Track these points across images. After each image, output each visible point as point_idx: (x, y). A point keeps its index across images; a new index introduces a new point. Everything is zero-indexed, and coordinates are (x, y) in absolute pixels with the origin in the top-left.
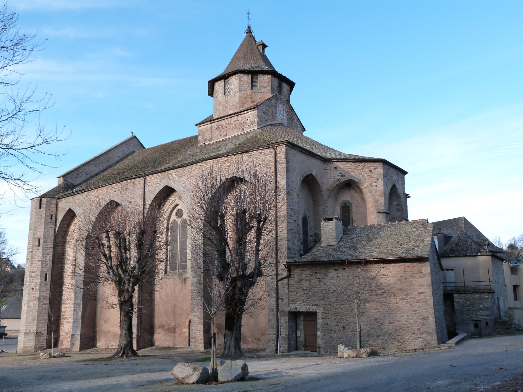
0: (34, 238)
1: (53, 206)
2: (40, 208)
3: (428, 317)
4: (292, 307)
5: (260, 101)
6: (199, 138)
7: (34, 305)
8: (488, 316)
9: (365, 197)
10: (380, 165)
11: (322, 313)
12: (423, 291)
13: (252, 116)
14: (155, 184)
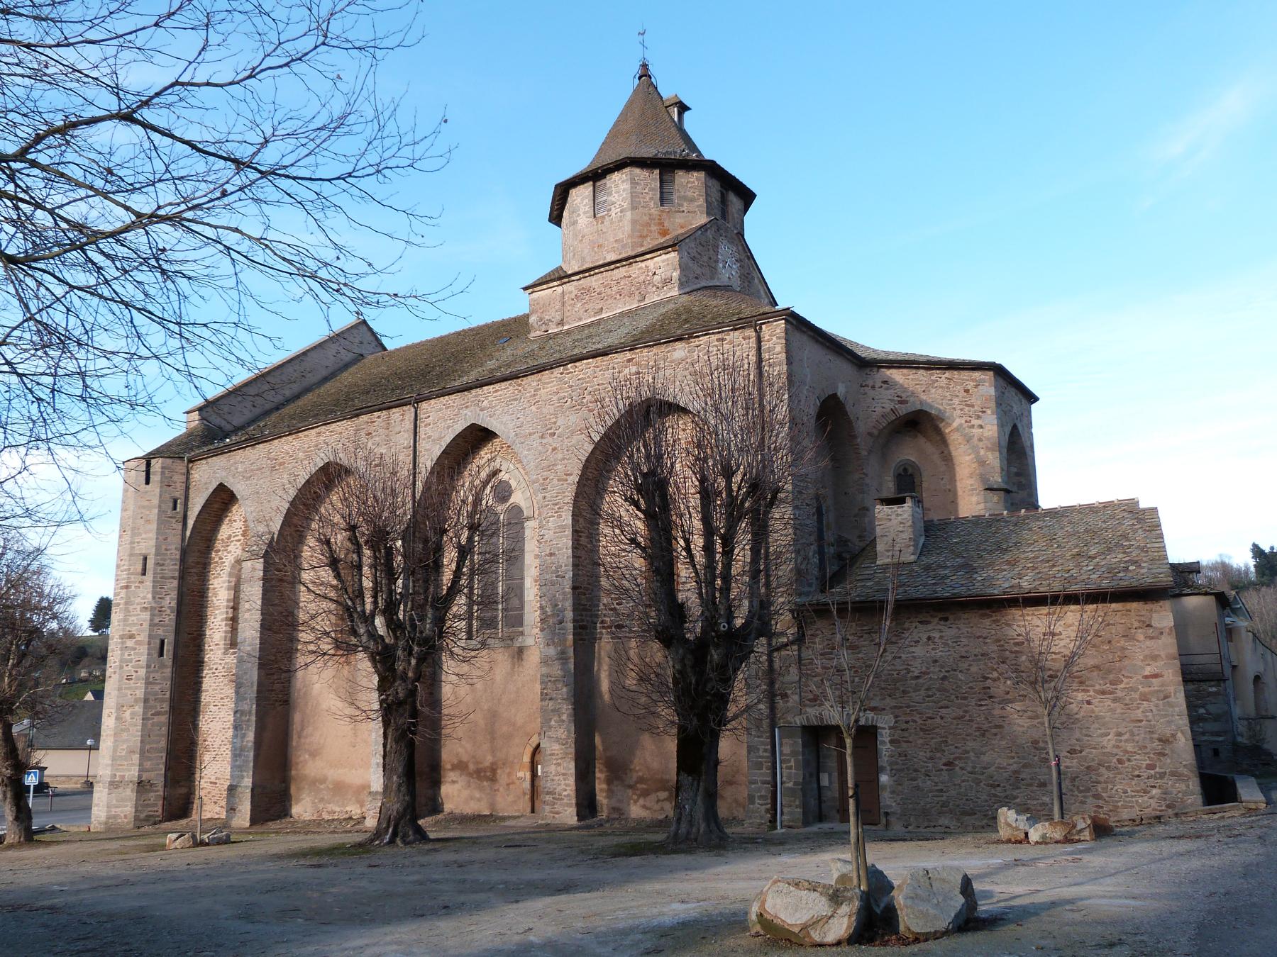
0: (131, 555)
1: (179, 479)
2: (147, 482)
3: (1173, 736)
4: (812, 714)
5: (682, 231)
6: (533, 319)
7: (133, 715)
8: (1218, 734)
9: (954, 453)
10: (988, 376)
11: (890, 728)
12: (1157, 671)
13: (666, 265)
14: (443, 420)
